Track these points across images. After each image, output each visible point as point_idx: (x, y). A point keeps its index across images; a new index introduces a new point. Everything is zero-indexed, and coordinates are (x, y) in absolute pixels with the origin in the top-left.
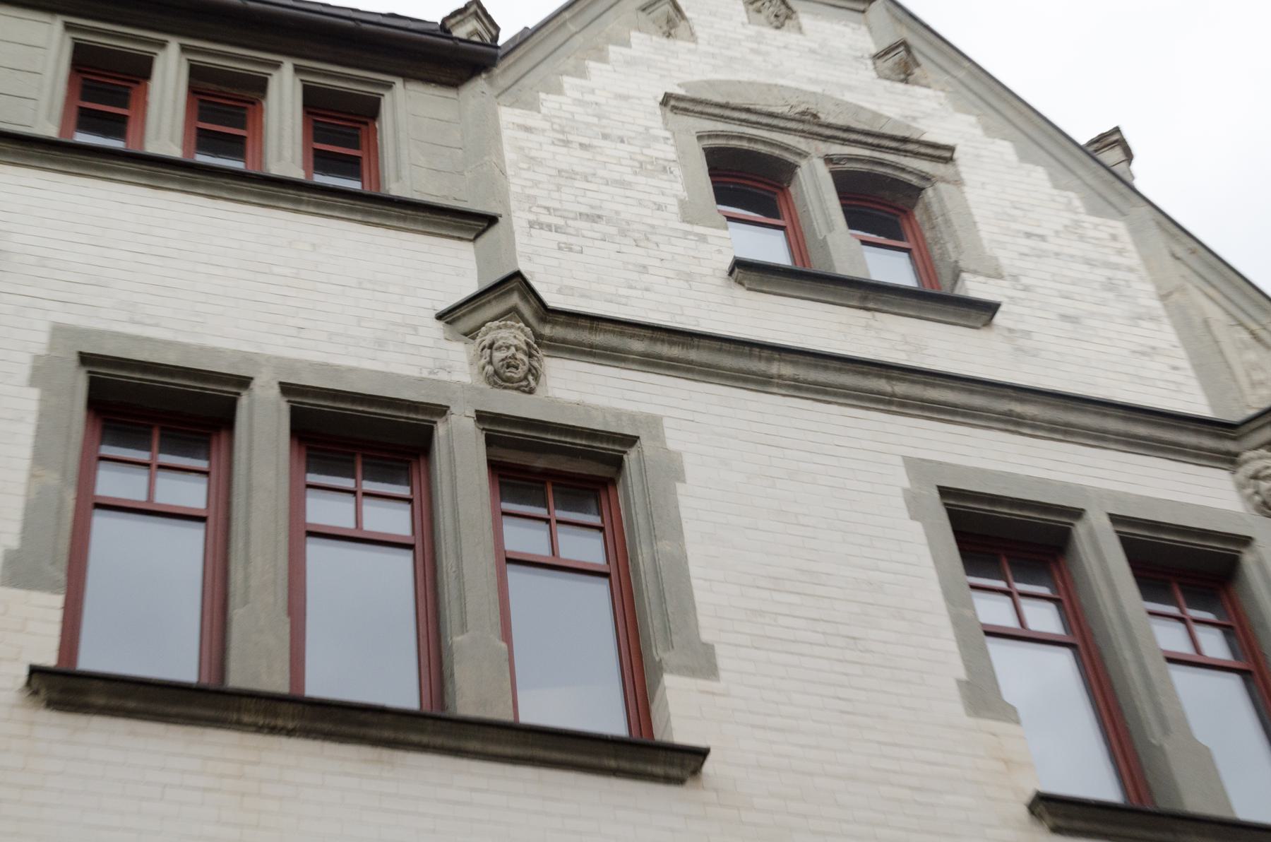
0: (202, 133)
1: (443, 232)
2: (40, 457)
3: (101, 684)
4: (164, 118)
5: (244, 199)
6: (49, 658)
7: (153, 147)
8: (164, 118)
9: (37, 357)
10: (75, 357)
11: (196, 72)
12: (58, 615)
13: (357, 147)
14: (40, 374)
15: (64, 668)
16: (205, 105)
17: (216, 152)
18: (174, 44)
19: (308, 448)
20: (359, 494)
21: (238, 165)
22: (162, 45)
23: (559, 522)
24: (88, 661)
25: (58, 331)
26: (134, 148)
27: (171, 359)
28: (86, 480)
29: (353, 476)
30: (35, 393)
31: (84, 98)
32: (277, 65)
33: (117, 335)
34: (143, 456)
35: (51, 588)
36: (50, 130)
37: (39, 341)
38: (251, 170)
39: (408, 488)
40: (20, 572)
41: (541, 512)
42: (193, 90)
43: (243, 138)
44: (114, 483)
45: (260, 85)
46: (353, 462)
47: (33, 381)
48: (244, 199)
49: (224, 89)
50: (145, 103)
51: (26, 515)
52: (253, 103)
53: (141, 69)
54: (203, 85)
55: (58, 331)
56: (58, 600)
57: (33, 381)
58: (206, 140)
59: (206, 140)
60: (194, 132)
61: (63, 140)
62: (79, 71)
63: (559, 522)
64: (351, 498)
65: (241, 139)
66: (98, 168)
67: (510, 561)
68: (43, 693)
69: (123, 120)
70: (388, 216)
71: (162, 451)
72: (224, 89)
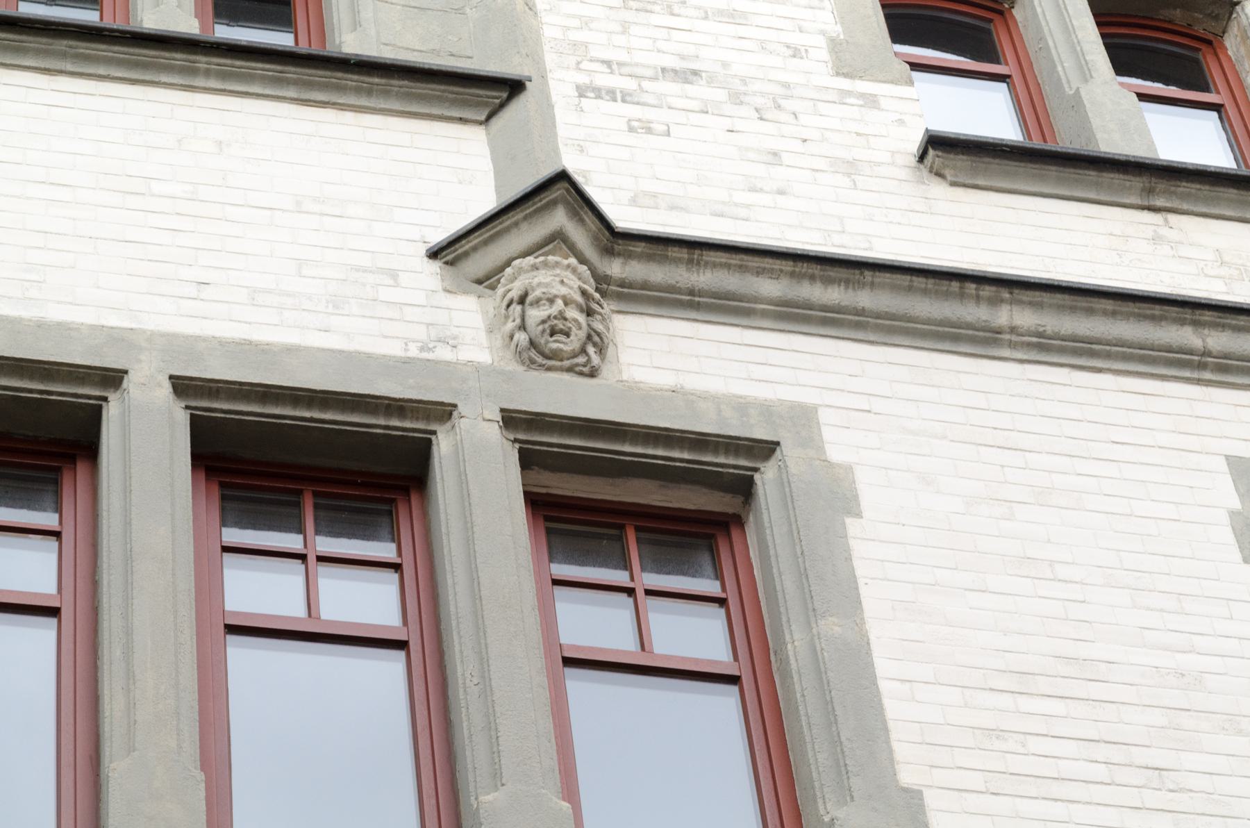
10: (167, 387)
19: (223, 485)
20: (312, 559)
21: (280, 39)
28: (208, 587)
29: (300, 530)
34: (291, 541)
38: (108, 23)
52: (1209, 43)
64: (297, 565)
67: (233, 629)
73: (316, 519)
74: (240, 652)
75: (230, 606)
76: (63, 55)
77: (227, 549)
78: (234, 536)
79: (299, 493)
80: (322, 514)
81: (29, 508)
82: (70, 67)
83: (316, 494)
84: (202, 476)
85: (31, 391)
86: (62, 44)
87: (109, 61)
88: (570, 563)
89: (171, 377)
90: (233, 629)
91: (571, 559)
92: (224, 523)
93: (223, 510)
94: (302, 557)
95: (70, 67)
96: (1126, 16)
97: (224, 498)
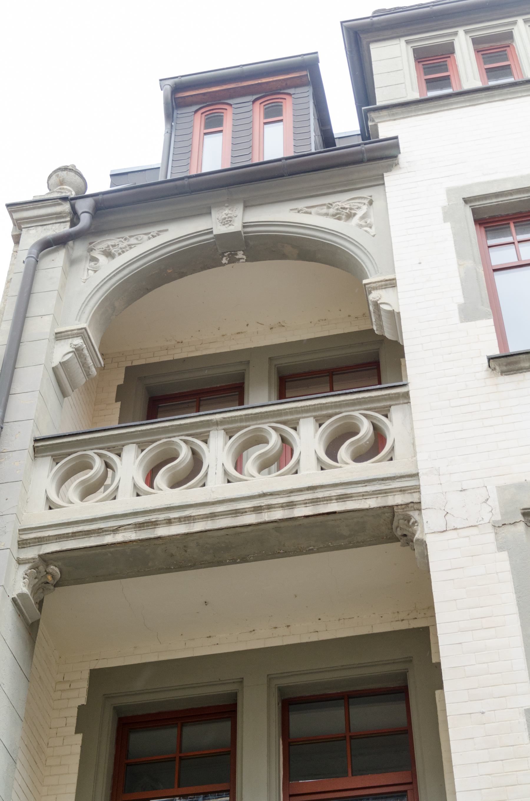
0: (488, 70)
1: (459, 106)
2: (460, 255)
3: (524, 356)
4: (467, 69)
5: (520, 95)
6: (496, 351)
7: (467, 86)
8: (467, 69)
9: (444, 208)
10: (462, 201)
11: (476, 41)
12: (493, 329)
13: (447, 71)
14: (448, 215)
15: (504, 354)
16: (485, 56)
17: (497, 78)
18: (461, 31)
19: (485, 228)
20: (516, 243)
21: (511, 80)
22: (456, 34)
23: (519, 242)
24: (513, 349)
25: (450, 191)
26: (457, 90)
27: (509, 187)
28: (485, 259)
29: (511, 235)
30: (448, 225)
31: (426, 74)
32: (515, 23)
33: (479, 184)
34: (509, 239)
35: (485, 317)
36: (415, 95)
37: (442, 200)
38: (517, 80)
39: (512, 237)
40: (467, 314)
41: (509, 239)
42: (477, 51)
43: (509, 65)
44: (501, 256)
45: (510, 36)
46: (509, 227)
47: (445, 220)
48: (520, 95)
49: (492, 44)
50: (456, 66)
51: (462, 285)
52: (509, 46)
53: (448, 50)
54: (481, 46)
55: (450, 191)
56: (491, 322)
57: (445, 220)
58: (491, 73)
59: (491, 73)
60: (484, 71)
61: (423, 98)
62: (419, 62)
63: (519, 242)
64: (512, 246)
65: (448, 78)
66: (444, 105)
67: (495, 270)
68: (497, 368)
69: (448, 78)
70: (478, 99)
71: (517, 234)
72: (492, 44)
73: (515, 230)
74: (499, 277)
75: (493, 264)
76: (507, 94)
77: (489, 247)
78: (491, 242)
79: (509, 224)
80: (517, 228)
81: (504, 237)
82: (510, 97)
83: (514, 223)
84: (478, 226)
85: (524, 197)
86: (505, 90)
87: (521, 91)
88: (495, 238)
89: (463, 198)
90: (495, 270)
91: (522, 233)
92: (487, 238)
93: (486, 235)
94: (513, 243)
95: (510, 97)
96: (435, 56)
97: (486, 231)
